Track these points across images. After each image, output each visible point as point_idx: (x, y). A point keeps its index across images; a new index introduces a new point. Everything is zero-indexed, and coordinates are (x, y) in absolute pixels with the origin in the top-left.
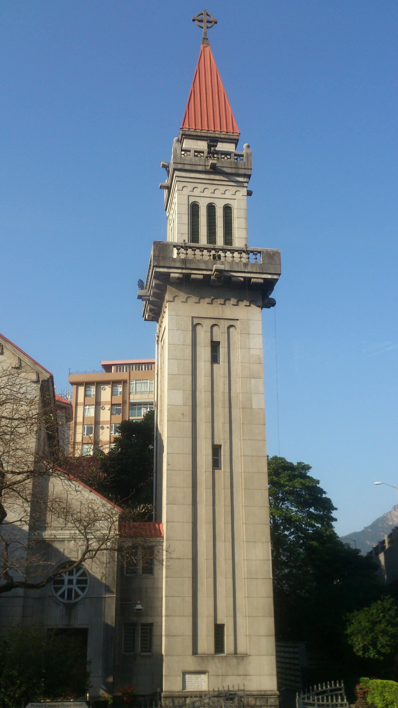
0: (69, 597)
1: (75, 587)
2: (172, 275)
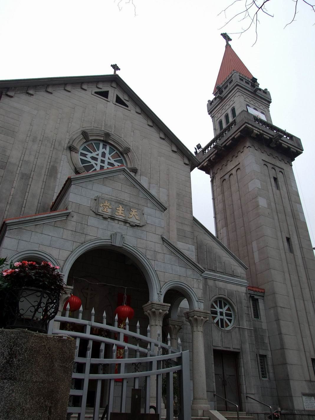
0: (222, 326)
1: (225, 318)
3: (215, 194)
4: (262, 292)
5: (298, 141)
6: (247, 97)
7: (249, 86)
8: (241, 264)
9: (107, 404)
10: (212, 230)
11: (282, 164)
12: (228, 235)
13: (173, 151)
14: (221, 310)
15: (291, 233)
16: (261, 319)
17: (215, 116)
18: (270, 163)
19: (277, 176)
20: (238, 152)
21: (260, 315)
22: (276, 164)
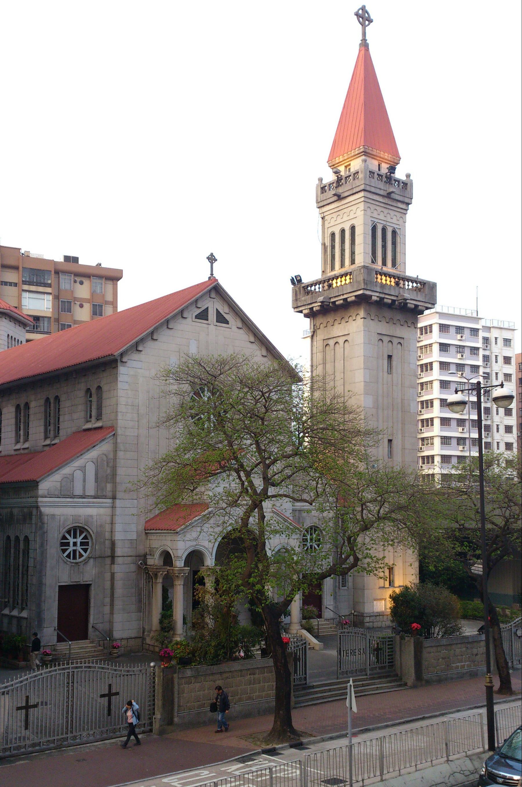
0: (75, 558)
1: (79, 548)
2: (385, 300)
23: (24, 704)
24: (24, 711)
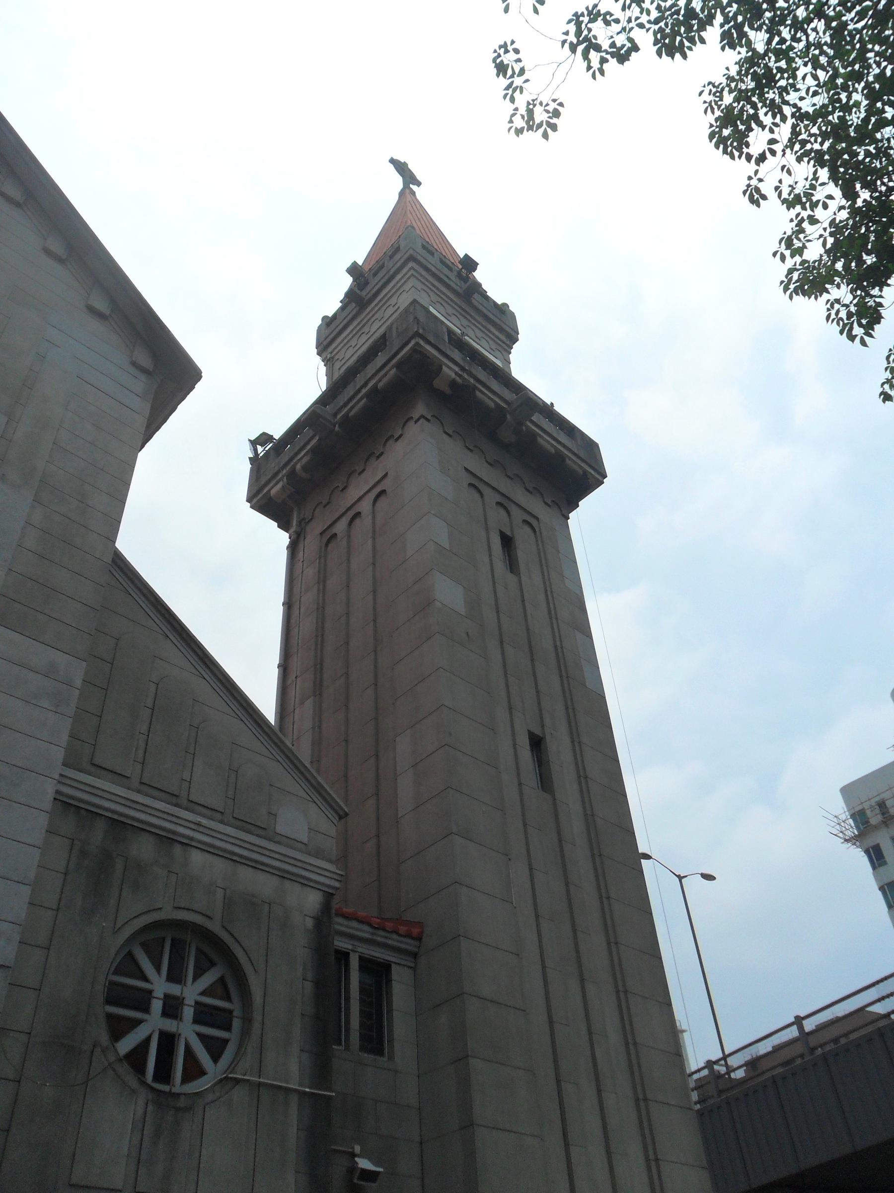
0: (164, 1073)
1: (187, 1030)
3: (296, 589)
4: (409, 935)
5: (591, 448)
6: (440, 300)
7: (455, 282)
8: (318, 789)
9: (832, 1044)
10: (266, 702)
11: (535, 505)
12: (318, 726)
13: (91, 310)
14: (175, 989)
15: (547, 721)
16: (391, 1058)
17: (337, 357)
18: (494, 488)
19: (512, 530)
20: (387, 440)
21: (391, 1041)
22: (512, 496)
23: (721, 1055)
24: (727, 1053)
